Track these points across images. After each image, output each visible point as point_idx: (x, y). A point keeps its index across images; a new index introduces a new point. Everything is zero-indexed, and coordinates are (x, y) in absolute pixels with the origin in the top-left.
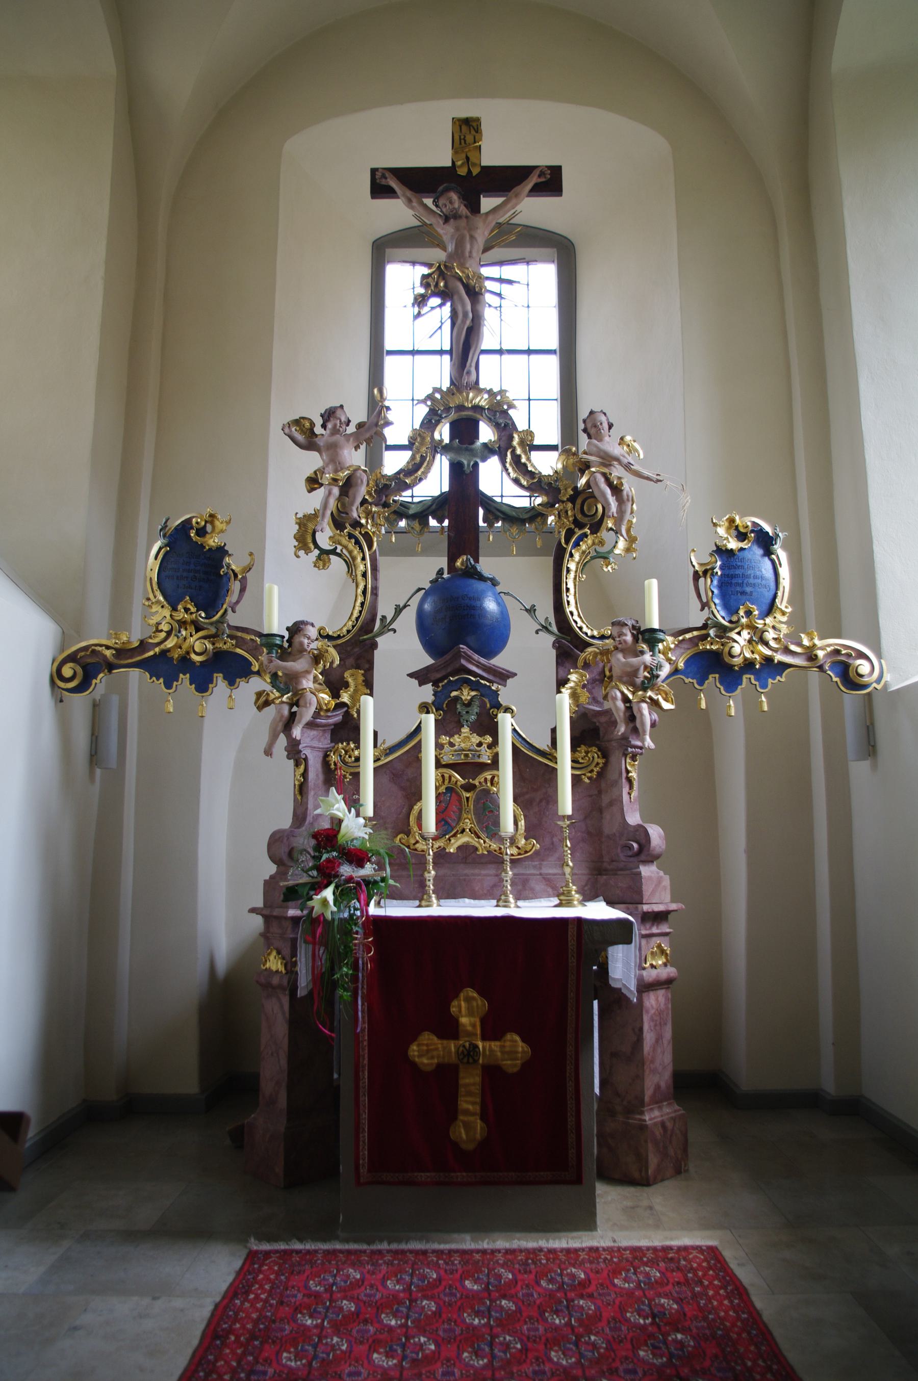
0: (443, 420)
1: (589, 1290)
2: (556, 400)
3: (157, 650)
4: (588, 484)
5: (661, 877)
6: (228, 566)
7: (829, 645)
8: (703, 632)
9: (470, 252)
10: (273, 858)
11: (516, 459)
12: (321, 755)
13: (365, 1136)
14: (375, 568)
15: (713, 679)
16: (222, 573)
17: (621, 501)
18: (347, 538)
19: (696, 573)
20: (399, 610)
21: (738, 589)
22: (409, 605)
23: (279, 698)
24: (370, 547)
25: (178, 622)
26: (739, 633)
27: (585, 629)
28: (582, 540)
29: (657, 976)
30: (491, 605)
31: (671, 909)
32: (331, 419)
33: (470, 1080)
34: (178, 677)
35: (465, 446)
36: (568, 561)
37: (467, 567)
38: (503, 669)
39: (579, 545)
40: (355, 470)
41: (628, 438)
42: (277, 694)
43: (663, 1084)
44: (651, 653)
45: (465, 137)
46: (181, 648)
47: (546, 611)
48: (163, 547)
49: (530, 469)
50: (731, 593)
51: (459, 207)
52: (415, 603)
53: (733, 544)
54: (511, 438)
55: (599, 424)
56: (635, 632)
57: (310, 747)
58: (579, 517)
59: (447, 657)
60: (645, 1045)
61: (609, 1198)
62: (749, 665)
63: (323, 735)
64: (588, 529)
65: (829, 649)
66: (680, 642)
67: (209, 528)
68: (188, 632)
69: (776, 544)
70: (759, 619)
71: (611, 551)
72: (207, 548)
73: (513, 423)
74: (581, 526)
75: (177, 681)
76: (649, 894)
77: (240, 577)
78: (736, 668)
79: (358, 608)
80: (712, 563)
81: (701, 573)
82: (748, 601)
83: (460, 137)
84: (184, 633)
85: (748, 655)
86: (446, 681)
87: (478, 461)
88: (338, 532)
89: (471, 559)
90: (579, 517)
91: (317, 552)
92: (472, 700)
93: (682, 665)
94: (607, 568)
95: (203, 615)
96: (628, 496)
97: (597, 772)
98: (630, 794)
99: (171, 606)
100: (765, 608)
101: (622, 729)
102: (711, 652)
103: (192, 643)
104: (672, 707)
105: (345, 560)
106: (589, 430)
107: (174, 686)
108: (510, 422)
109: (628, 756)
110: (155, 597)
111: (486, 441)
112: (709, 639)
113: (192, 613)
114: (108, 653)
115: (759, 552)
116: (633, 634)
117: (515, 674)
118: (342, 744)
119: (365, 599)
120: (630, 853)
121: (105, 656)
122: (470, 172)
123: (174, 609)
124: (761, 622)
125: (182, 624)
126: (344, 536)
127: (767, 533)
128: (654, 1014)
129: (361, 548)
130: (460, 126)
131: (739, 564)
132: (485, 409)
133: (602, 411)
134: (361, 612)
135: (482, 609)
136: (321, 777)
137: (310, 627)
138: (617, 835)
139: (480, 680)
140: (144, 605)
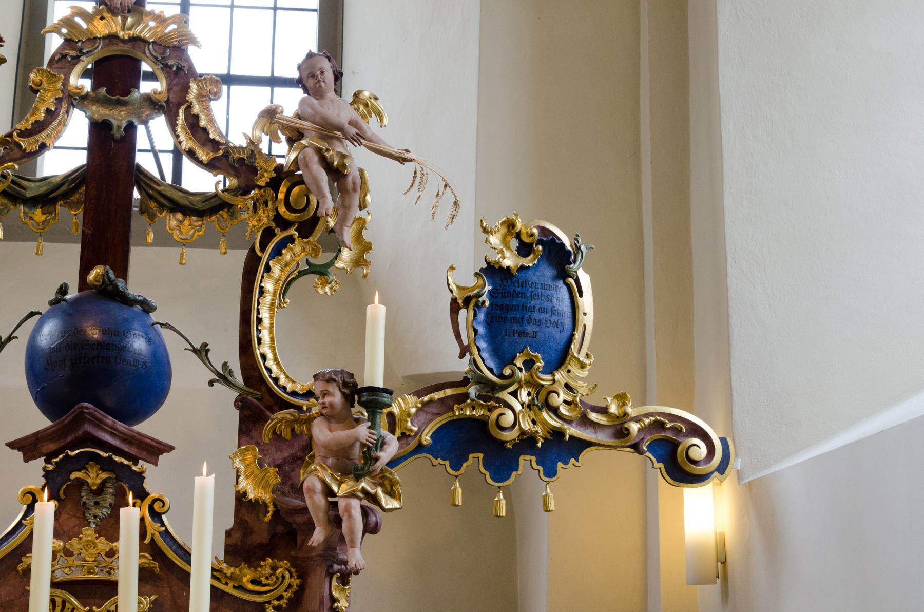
0: (83, 58)
7: (647, 415)
8: (460, 390)
11: (193, 124)
19: (454, 301)
21: (516, 327)
22: (17, 338)
26: (514, 394)
28: (285, 247)
30: (139, 344)
36: (263, 277)
37: (104, 282)
38: (153, 439)
39: (281, 254)
41: (366, 94)
44: (369, 424)
49: (211, 136)
50: (504, 333)
53: (509, 261)
54: (186, 89)
55: (318, 73)
56: (347, 391)
58: (282, 210)
62: (527, 442)
64: (296, 230)
65: (647, 421)
69: (575, 262)
70: (543, 372)
74: (284, 224)
81: (460, 301)
82: (530, 346)
85: (526, 425)
86: (61, 457)
90: (282, 210)
93: (428, 438)
97: (289, 599)
100: (554, 355)
101: (318, 536)
102: (472, 419)
108: (186, 64)
112: (469, 401)
115: (548, 272)
116: (343, 394)
124: (548, 377)
127: (562, 245)
131: (518, 289)
132: (149, 43)
139: (114, 457)
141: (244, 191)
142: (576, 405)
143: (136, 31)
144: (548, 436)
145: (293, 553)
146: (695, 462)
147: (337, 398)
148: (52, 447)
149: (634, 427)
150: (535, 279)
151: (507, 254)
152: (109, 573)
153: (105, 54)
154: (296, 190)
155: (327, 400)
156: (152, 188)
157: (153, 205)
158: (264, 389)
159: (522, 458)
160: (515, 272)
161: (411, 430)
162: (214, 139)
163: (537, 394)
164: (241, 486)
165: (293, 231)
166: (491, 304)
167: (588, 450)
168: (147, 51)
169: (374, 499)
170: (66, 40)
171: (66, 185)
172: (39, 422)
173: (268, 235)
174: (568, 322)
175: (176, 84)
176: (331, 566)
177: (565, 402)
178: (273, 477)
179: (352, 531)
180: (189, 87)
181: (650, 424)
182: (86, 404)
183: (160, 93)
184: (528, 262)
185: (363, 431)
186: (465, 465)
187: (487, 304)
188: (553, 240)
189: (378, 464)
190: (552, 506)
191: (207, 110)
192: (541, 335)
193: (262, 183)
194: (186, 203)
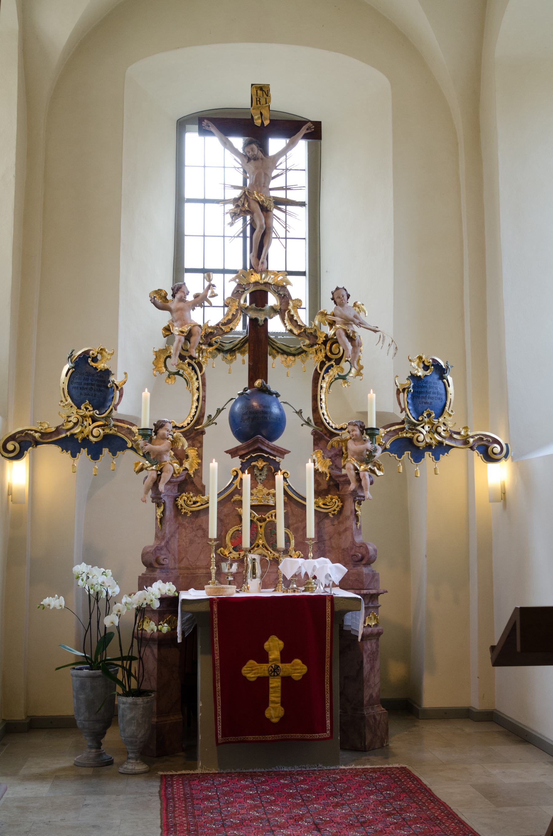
0: (245, 292)
2: (305, 239)
3: (68, 433)
6: (113, 382)
7: (476, 435)
9: (264, 183)
10: (145, 563)
11: (291, 318)
12: (173, 499)
13: (219, 718)
14: (204, 384)
15: (407, 454)
16: (109, 386)
17: (353, 345)
18: (187, 365)
19: (398, 390)
20: (219, 411)
21: (424, 400)
23: (151, 466)
24: (201, 371)
25: (81, 416)
26: (423, 427)
27: (331, 424)
28: (330, 369)
30: (275, 410)
32: (179, 292)
33: (275, 683)
34: (80, 450)
35: (259, 308)
36: (322, 382)
37: (262, 386)
38: (282, 449)
39: (328, 372)
40: (194, 326)
41: (359, 303)
42: (149, 465)
44: (371, 442)
45: (260, 99)
46: (83, 432)
47: (308, 413)
48: (71, 369)
49: (299, 324)
51: (258, 153)
53: (420, 373)
54: (288, 304)
56: (361, 429)
57: (167, 495)
58: (329, 354)
59: (250, 441)
60: (364, 671)
62: (429, 447)
63: (174, 488)
65: (476, 438)
66: (388, 432)
67: (99, 357)
68: (88, 422)
69: (446, 373)
70: (435, 418)
71: (347, 375)
72: (99, 370)
73: (289, 294)
74: (329, 359)
76: (368, 583)
77: (120, 388)
78: (421, 448)
79: (194, 410)
80: (408, 384)
81: (401, 390)
83: (257, 98)
84: (85, 423)
85: (428, 440)
86: (249, 456)
87: (268, 318)
88: (182, 361)
89: (264, 382)
90: (329, 354)
91: (167, 373)
92: (263, 467)
93: (389, 446)
94: (344, 385)
95: (98, 412)
96: (358, 343)
97: (338, 511)
99: (76, 406)
100: (439, 412)
101: (353, 486)
102: (406, 438)
103: (91, 430)
104: (382, 474)
105: (185, 379)
106: (335, 299)
108: (286, 293)
109: (356, 502)
110: (66, 400)
111: (272, 305)
112: (405, 431)
113: (90, 411)
114: (37, 435)
115: (436, 377)
116: (360, 430)
117: (290, 452)
118: (185, 493)
119: (198, 404)
120: (357, 559)
121: (35, 437)
122: (262, 123)
123: (79, 408)
124: (436, 420)
125: (84, 417)
126: (185, 365)
127: (442, 366)
128: (370, 653)
129: (196, 372)
130: (257, 91)
131: (424, 385)
133: (343, 287)
134: (196, 412)
135: (271, 413)
136: (173, 513)
137: (168, 424)
138: (349, 548)
140: (60, 405)
141: (312, 346)
142: (448, 431)
143: (266, 280)
144: (437, 444)
145: (338, 493)
146: (495, 454)
147: (358, 432)
148: (243, 452)
149: (471, 440)
150: (430, 380)
151: (420, 370)
152: (268, 502)
153: (253, 290)
154: (334, 346)
155: (354, 433)
156: (274, 345)
157: (274, 352)
158: (323, 427)
159: (426, 453)
160: (422, 377)
161: (382, 443)
162: (300, 325)
163: (432, 427)
164: (316, 467)
165: (333, 362)
166: (413, 391)
167: (452, 449)
168: (271, 288)
169: (373, 472)
170: (238, 284)
171: (240, 344)
172: (236, 443)
173: (322, 364)
174: (444, 397)
175: (284, 302)
176: (355, 498)
177: (444, 430)
178: (328, 462)
179: (366, 484)
180: (289, 303)
181: (478, 439)
182: (259, 436)
183: (277, 306)
184: (428, 373)
185: (369, 445)
186: (403, 456)
187: (412, 391)
188: (438, 364)
189: (375, 458)
190: (438, 472)
191: (296, 312)
192: (433, 403)
193: (320, 343)
194: (289, 351)
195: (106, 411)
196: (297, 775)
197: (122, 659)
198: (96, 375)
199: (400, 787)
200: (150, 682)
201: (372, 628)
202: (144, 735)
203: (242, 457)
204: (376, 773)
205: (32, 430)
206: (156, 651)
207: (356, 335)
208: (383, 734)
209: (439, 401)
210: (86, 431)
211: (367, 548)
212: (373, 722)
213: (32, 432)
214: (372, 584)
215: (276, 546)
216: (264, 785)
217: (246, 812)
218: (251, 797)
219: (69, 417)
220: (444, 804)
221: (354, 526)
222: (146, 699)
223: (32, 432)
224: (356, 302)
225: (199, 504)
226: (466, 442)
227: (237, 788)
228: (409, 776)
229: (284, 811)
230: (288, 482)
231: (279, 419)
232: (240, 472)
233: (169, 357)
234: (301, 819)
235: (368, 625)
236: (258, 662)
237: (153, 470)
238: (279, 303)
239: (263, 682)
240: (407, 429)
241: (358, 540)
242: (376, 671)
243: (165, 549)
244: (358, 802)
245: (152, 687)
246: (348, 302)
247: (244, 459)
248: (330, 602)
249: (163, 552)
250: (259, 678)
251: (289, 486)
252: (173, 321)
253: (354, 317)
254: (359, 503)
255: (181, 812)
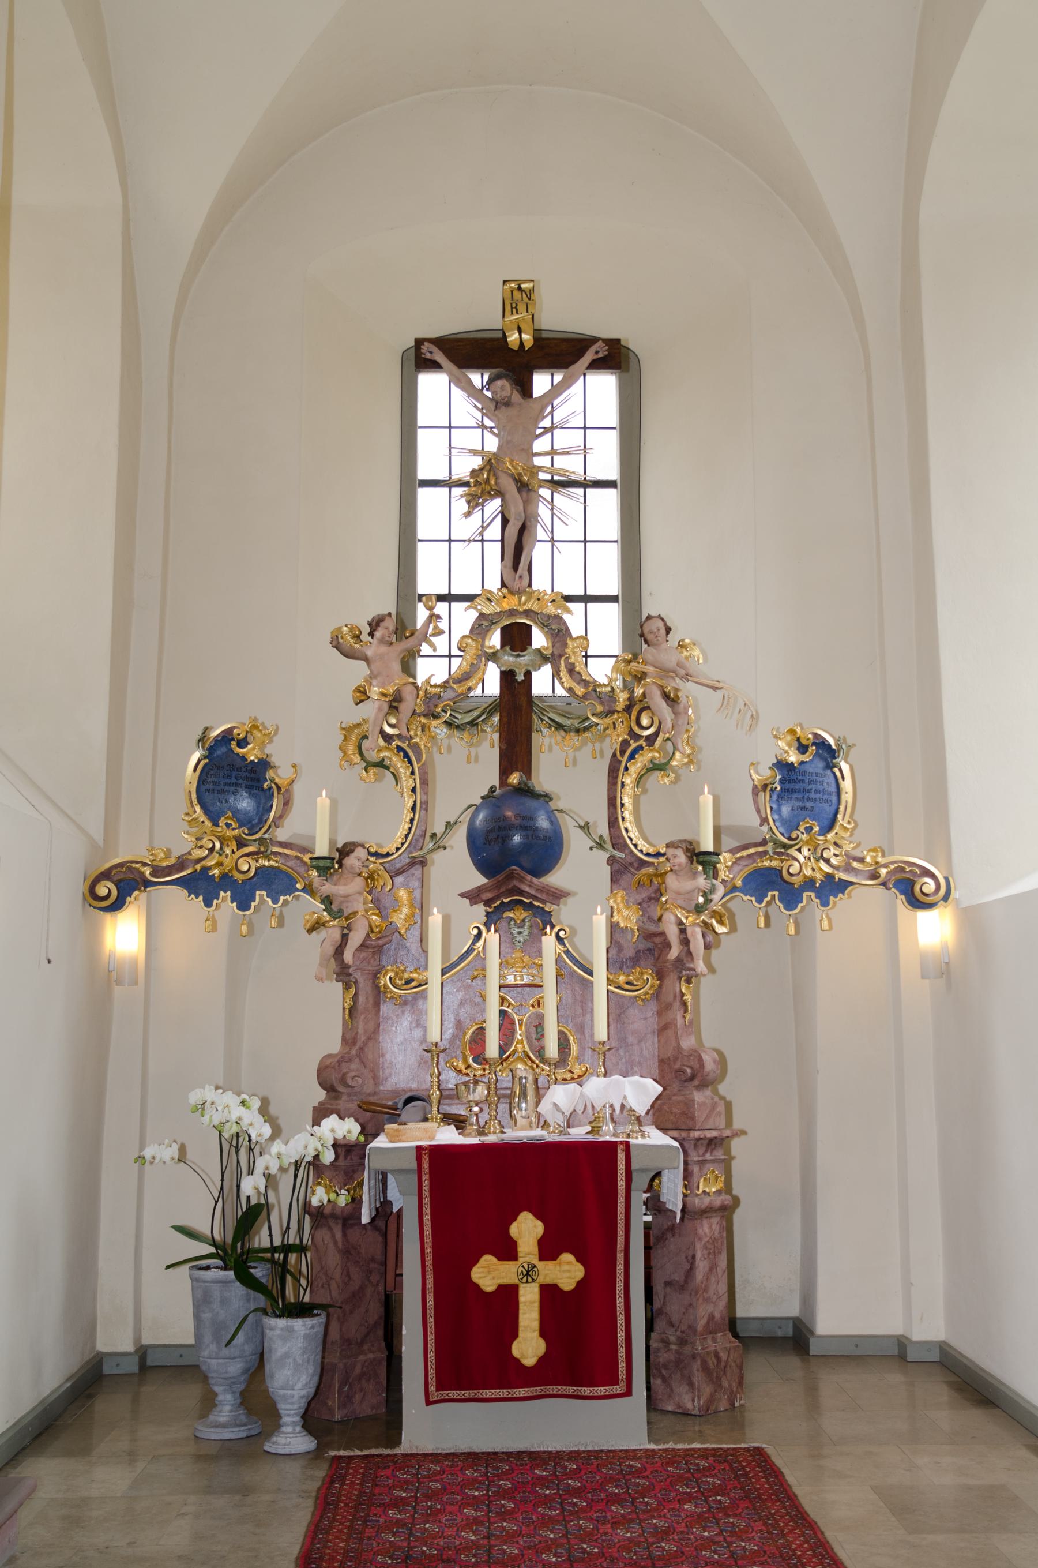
1: (646, 1474)
4: (644, 695)
5: (716, 1103)
6: (272, 781)
7: (892, 863)
8: (761, 849)
10: (322, 1084)
11: (571, 670)
14: (424, 782)
19: (755, 787)
24: (419, 760)
26: (799, 850)
29: (710, 1203)
31: (725, 1135)
32: (380, 629)
33: (529, 1297)
34: (219, 895)
39: (634, 758)
42: (328, 918)
43: (717, 1315)
45: (517, 305)
47: (603, 829)
52: (466, 818)
53: (793, 758)
57: (360, 969)
59: (500, 877)
60: (697, 1273)
61: (662, 1425)
62: (809, 883)
65: (892, 867)
66: (738, 859)
69: (839, 756)
70: (819, 835)
73: (567, 629)
75: (218, 899)
77: (283, 790)
81: (759, 787)
83: (511, 304)
85: (808, 872)
91: (364, 764)
95: (246, 831)
98: (684, 1017)
100: (826, 823)
101: (674, 952)
102: (770, 868)
105: (393, 773)
107: (214, 904)
108: (563, 627)
111: (539, 647)
113: (233, 829)
114: (147, 871)
115: (821, 764)
123: (216, 824)
124: (821, 838)
127: (829, 745)
128: (708, 1242)
129: (410, 762)
131: (800, 778)
146: (926, 895)
148: (488, 895)
149: (883, 871)
150: (811, 770)
155: (677, 861)
156: (544, 715)
163: (815, 850)
165: (642, 742)
166: (781, 789)
174: (834, 799)
176: (681, 972)
181: (896, 868)
183: (547, 648)
184: (806, 758)
187: (779, 789)
189: (712, 903)
195: (261, 829)
196: (567, 1461)
197: (273, 1249)
198: (244, 769)
199: (742, 1488)
200: (330, 1290)
201: (712, 1198)
202: (306, 1385)
203: (487, 903)
204: (707, 1459)
205: (137, 862)
206: (339, 1235)
207: (680, 694)
208: (734, 1384)
209: (826, 806)
210: (228, 863)
211: (700, 1060)
212: (713, 1363)
213: (137, 866)
214: (712, 1119)
215: (544, 1055)
216: (503, 1480)
217: (454, 1534)
218: (474, 1502)
219: (199, 839)
220: (812, 1525)
221: (679, 1021)
222: (309, 1322)
223: (137, 866)
224: (683, 640)
225: (413, 984)
226: (874, 876)
227: (455, 1485)
228: (765, 1466)
229: (523, 1533)
230: (567, 945)
231: (550, 838)
232: (483, 929)
233: (366, 737)
234: (548, 1549)
235: (704, 1192)
236: (499, 1259)
237: (334, 926)
238: (550, 645)
239: (508, 1294)
240: (771, 853)
241: (687, 1043)
242: (720, 1273)
243: (357, 1060)
244: (660, 1517)
245: (332, 1298)
246: (667, 641)
247: (490, 907)
248: (624, 1154)
249: (353, 1066)
250: (501, 1287)
251: (567, 952)
252: (371, 677)
253: (678, 665)
254: (688, 981)
255: (341, 1531)
